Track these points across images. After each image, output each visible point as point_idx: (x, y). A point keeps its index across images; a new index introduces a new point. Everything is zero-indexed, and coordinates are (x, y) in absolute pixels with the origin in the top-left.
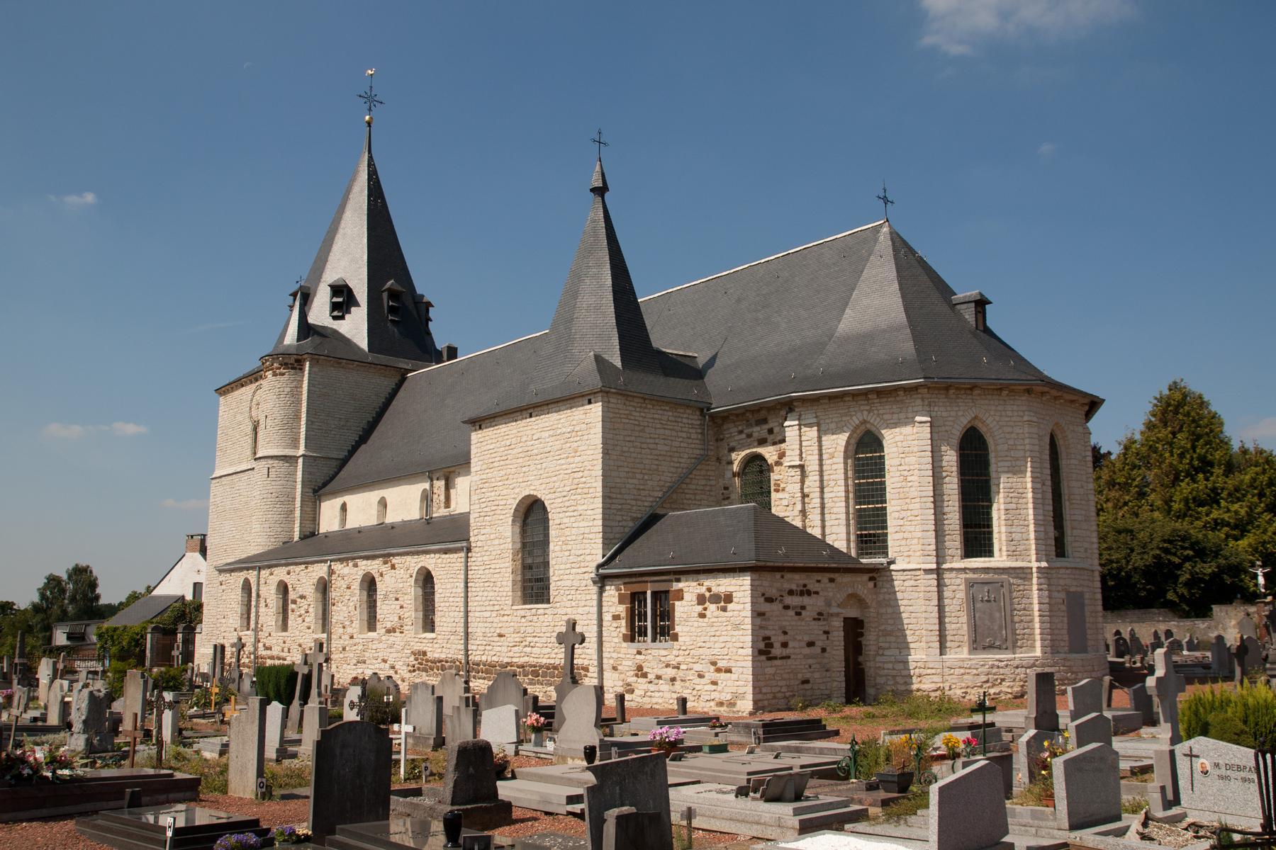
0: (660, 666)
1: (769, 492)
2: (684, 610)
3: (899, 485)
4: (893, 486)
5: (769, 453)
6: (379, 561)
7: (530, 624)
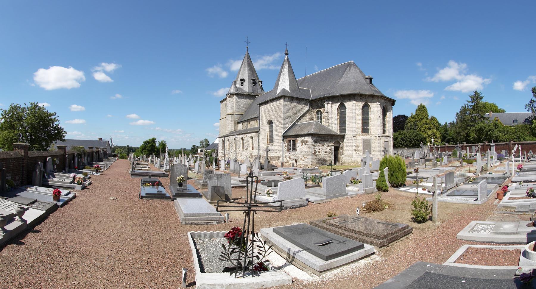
1: (322, 119)
2: (298, 144)
3: (348, 117)
5: (322, 110)
6: (244, 135)
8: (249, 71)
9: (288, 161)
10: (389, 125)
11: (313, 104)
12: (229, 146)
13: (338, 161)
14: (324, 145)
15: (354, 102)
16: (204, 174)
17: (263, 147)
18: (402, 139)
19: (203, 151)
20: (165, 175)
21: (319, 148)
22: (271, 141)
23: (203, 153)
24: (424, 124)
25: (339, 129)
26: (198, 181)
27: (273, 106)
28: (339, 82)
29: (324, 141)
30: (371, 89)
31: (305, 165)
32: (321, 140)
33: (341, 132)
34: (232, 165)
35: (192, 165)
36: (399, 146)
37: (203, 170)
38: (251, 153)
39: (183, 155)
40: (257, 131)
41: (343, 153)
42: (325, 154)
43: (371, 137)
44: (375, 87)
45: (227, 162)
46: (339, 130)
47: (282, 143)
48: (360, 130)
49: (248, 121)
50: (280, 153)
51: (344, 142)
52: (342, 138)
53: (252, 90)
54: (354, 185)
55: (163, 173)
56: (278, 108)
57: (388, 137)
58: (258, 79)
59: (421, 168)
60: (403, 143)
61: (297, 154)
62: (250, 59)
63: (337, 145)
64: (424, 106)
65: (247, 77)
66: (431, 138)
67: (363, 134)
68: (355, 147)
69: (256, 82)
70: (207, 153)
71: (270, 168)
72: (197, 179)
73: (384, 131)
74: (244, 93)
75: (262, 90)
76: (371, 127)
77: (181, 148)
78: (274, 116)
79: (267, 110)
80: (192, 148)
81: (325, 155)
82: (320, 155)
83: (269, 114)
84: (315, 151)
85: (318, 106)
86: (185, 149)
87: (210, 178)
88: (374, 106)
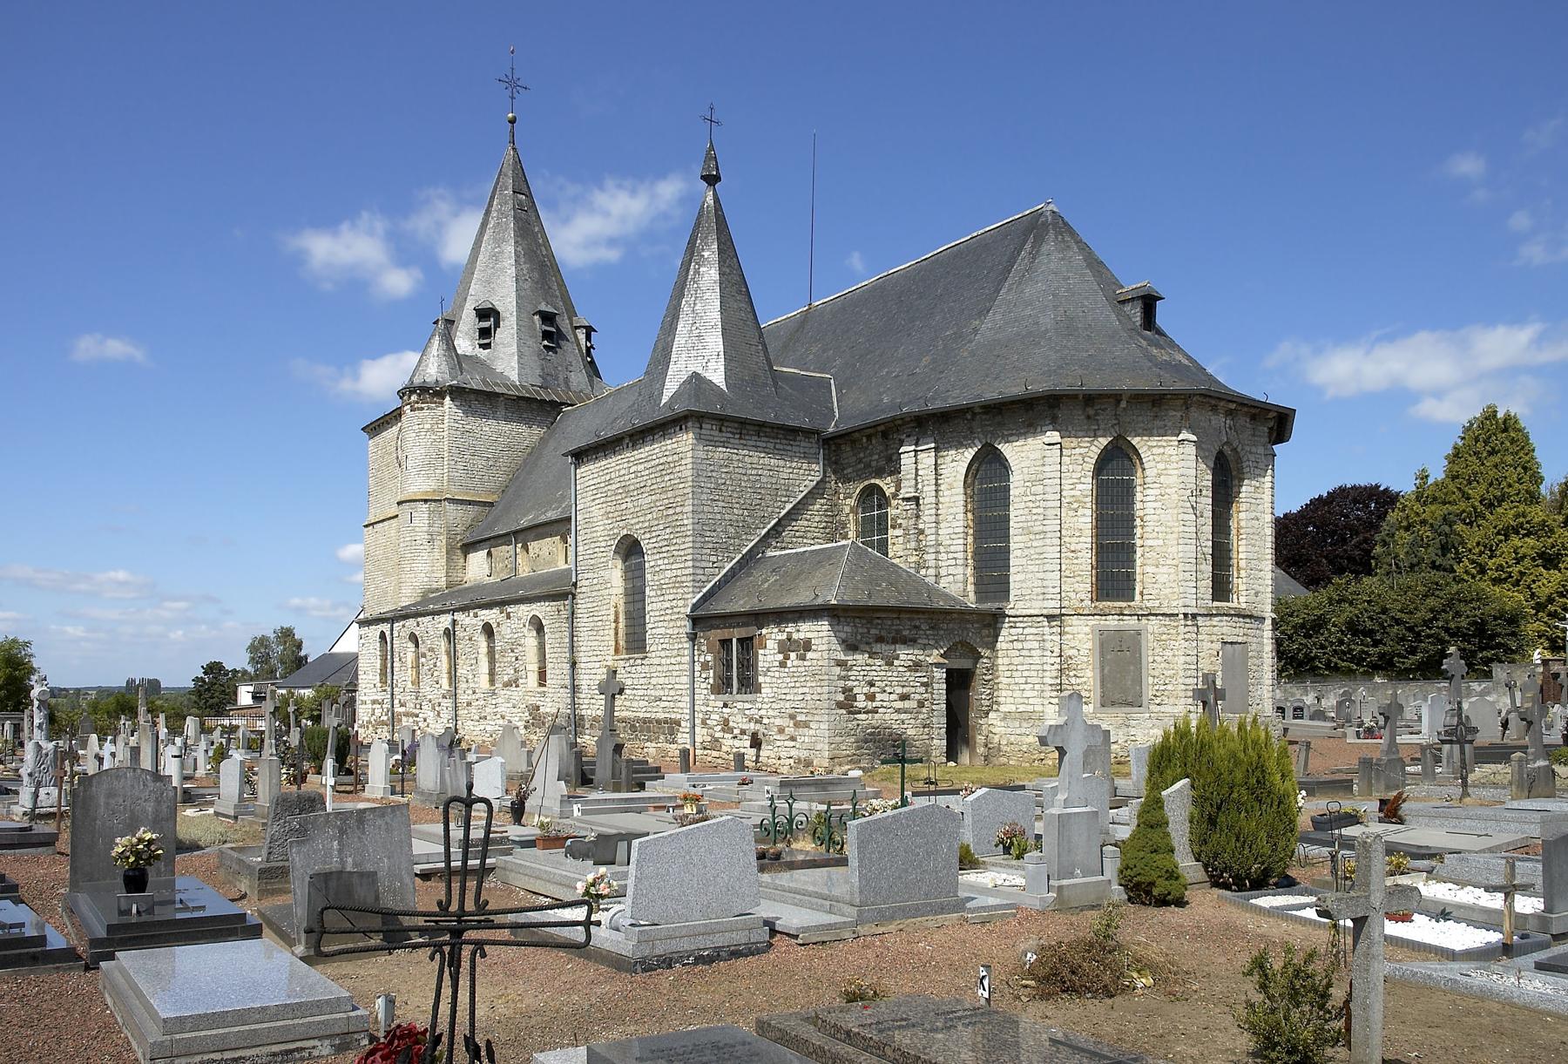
0: (745, 720)
2: (768, 656)
3: (1023, 518)
4: (1019, 519)
6: (496, 611)
7: (629, 675)
8: (525, 267)
9: (715, 744)
10: (1251, 556)
11: (844, 455)
12: (417, 666)
13: (968, 742)
14: (896, 663)
15: (1054, 436)
16: (272, 815)
17: (592, 675)
18: (1353, 627)
19: (264, 698)
20: (34, 840)
21: (867, 678)
22: (635, 641)
23: (268, 706)
24: (1507, 533)
25: (971, 580)
26: (235, 855)
27: (641, 467)
28: (976, 331)
29: (895, 641)
30: (1151, 358)
31: (799, 761)
32: (880, 640)
33: (981, 593)
34: (428, 770)
35: (201, 772)
36: (1336, 669)
37: (264, 796)
38: (533, 701)
39: (141, 719)
40: (562, 591)
41: (994, 703)
42: (899, 705)
43: (1144, 621)
44: (1173, 345)
45: (404, 753)
46: (971, 588)
47: (686, 652)
48: (1081, 586)
49: (521, 537)
50: (680, 705)
51: (999, 645)
52: (989, 625)
53: (538, 372)
54: (1014, 862)
55: (21, 829)
56: (667, 478)
57: (1244, 617)
58: (572, 313)
59: (1419, 795)
60: (1363, 652)
61: (759, 705)
62: (529, 196)
63: (961, 664)
64: (1507, 418)
65: (513, 307)
66: (1553, 615)
67: (1101, 605)
68: (1055, 674)
69: (558, 329)
70: (291, 709)
71: (623, 776)
72: (232, 848)
73: (1221, 588)
74: (497, 390)
75: (589, 376)
76: (1148, 569)
77: (130, 682)
78: (650, 516)
79: (614, 487)
80: (202, 680)
81: (898, 711)
82: (875, 711)
83: (624, 506)
84: (851, 690)
85: (868, 466)
86: (154, 686)
87: (302, 833)
88: (1161, 450)
